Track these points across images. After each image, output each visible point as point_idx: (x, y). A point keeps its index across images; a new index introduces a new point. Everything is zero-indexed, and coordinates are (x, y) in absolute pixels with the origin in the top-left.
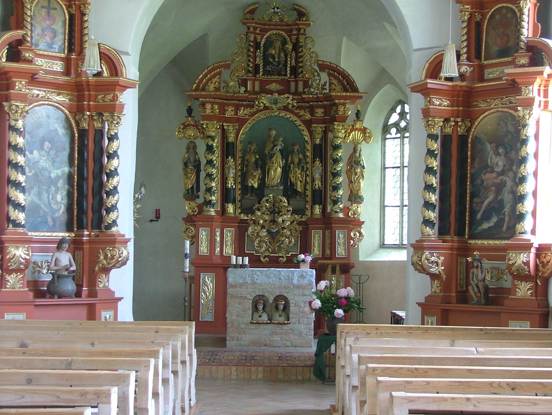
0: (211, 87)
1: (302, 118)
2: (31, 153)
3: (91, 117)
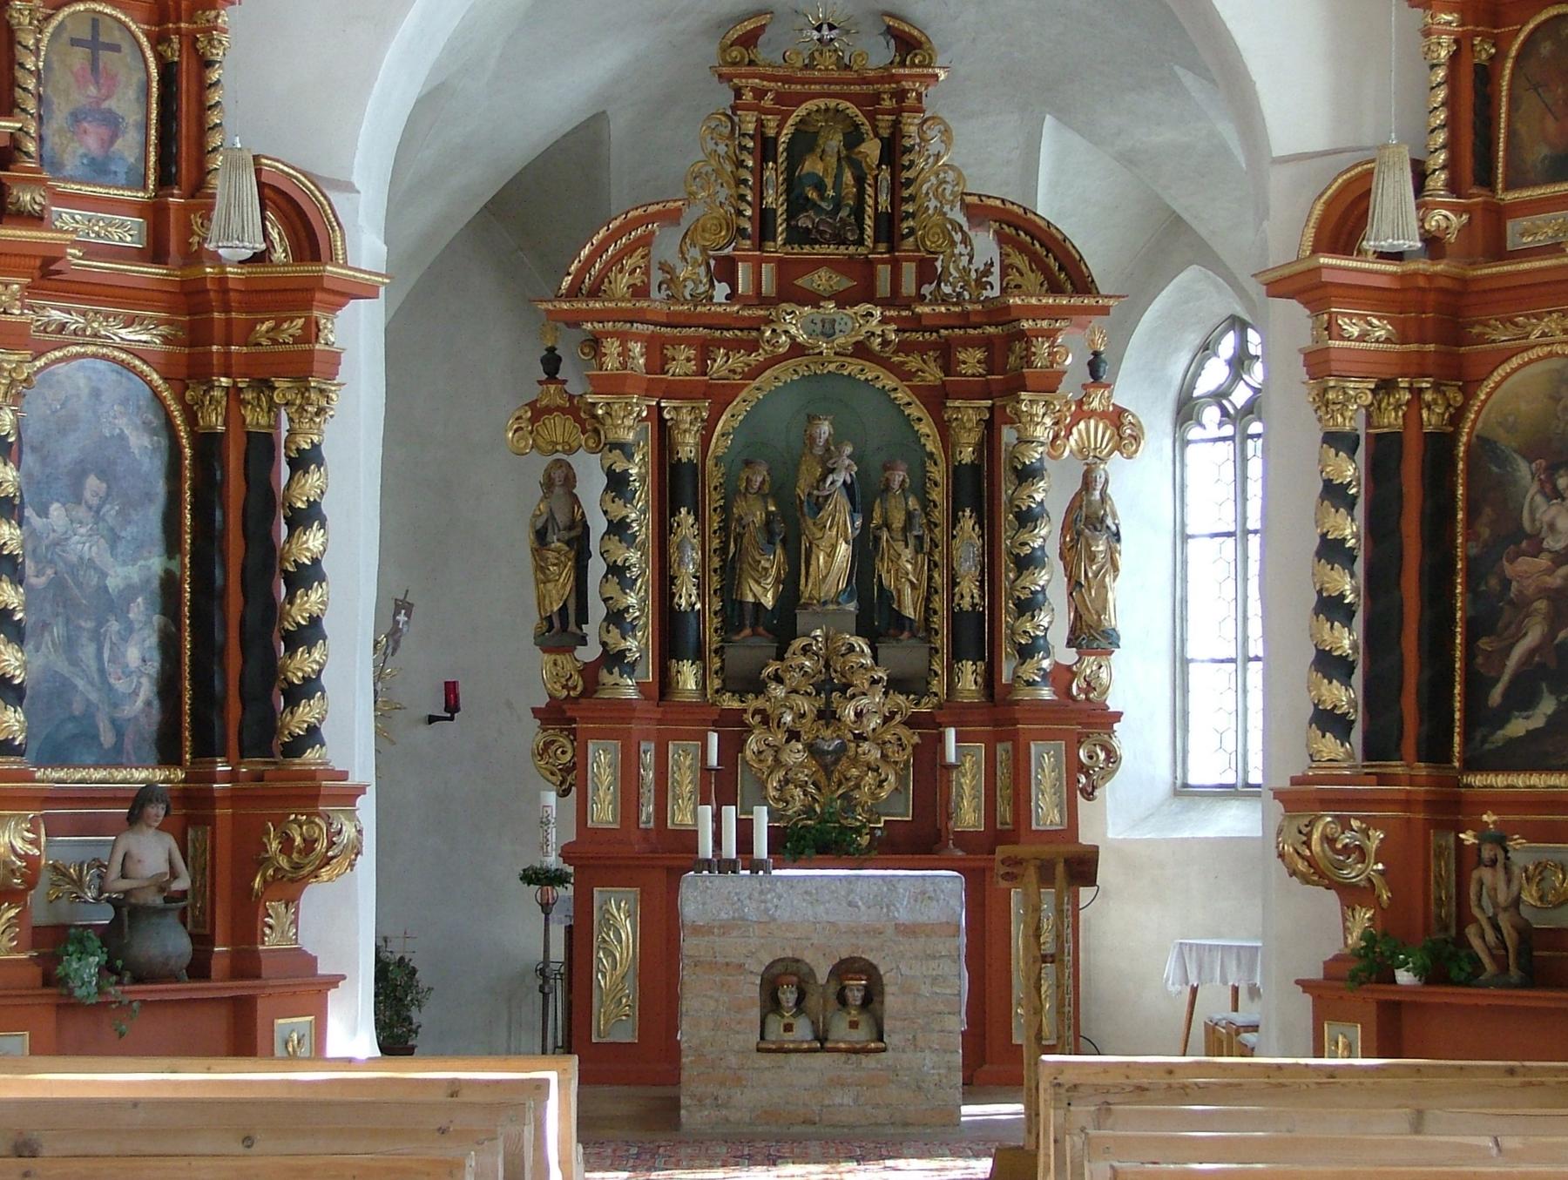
0: (622, 283)
1: (916, 382)
2: (43, 512)
3: (233, 393)
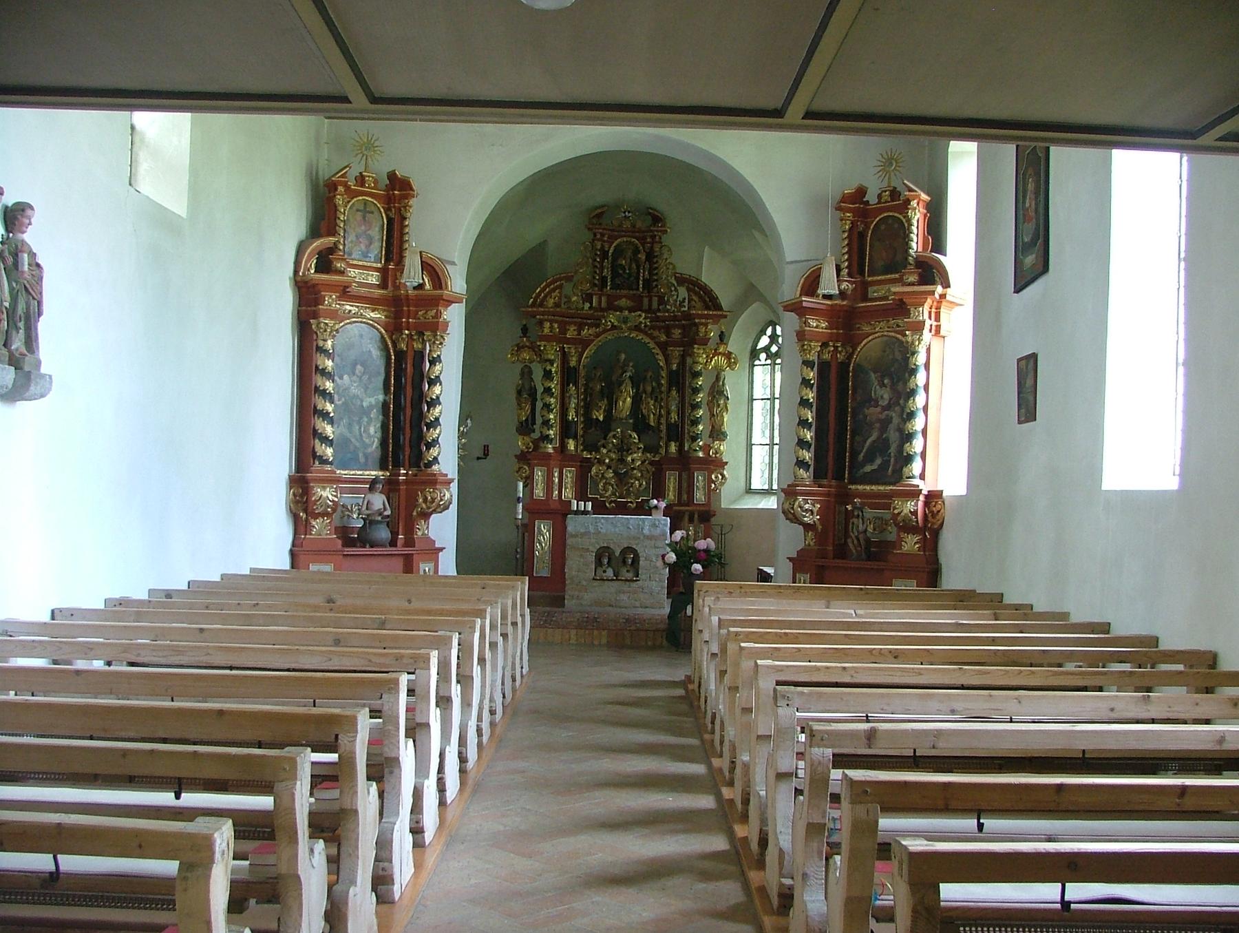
2: (341, 378)
3: (410, 336)
